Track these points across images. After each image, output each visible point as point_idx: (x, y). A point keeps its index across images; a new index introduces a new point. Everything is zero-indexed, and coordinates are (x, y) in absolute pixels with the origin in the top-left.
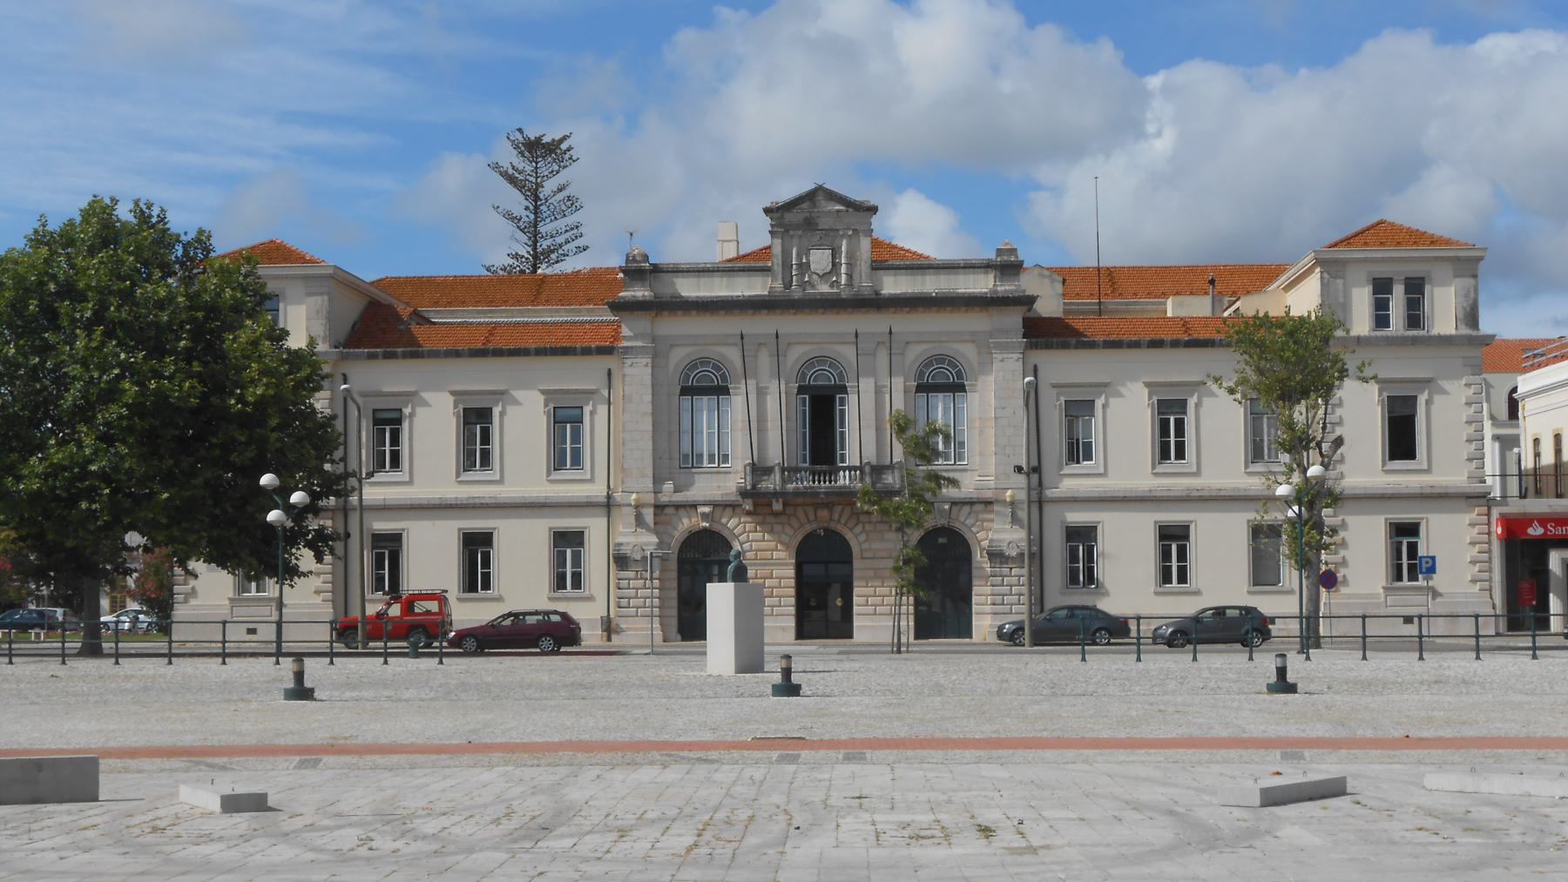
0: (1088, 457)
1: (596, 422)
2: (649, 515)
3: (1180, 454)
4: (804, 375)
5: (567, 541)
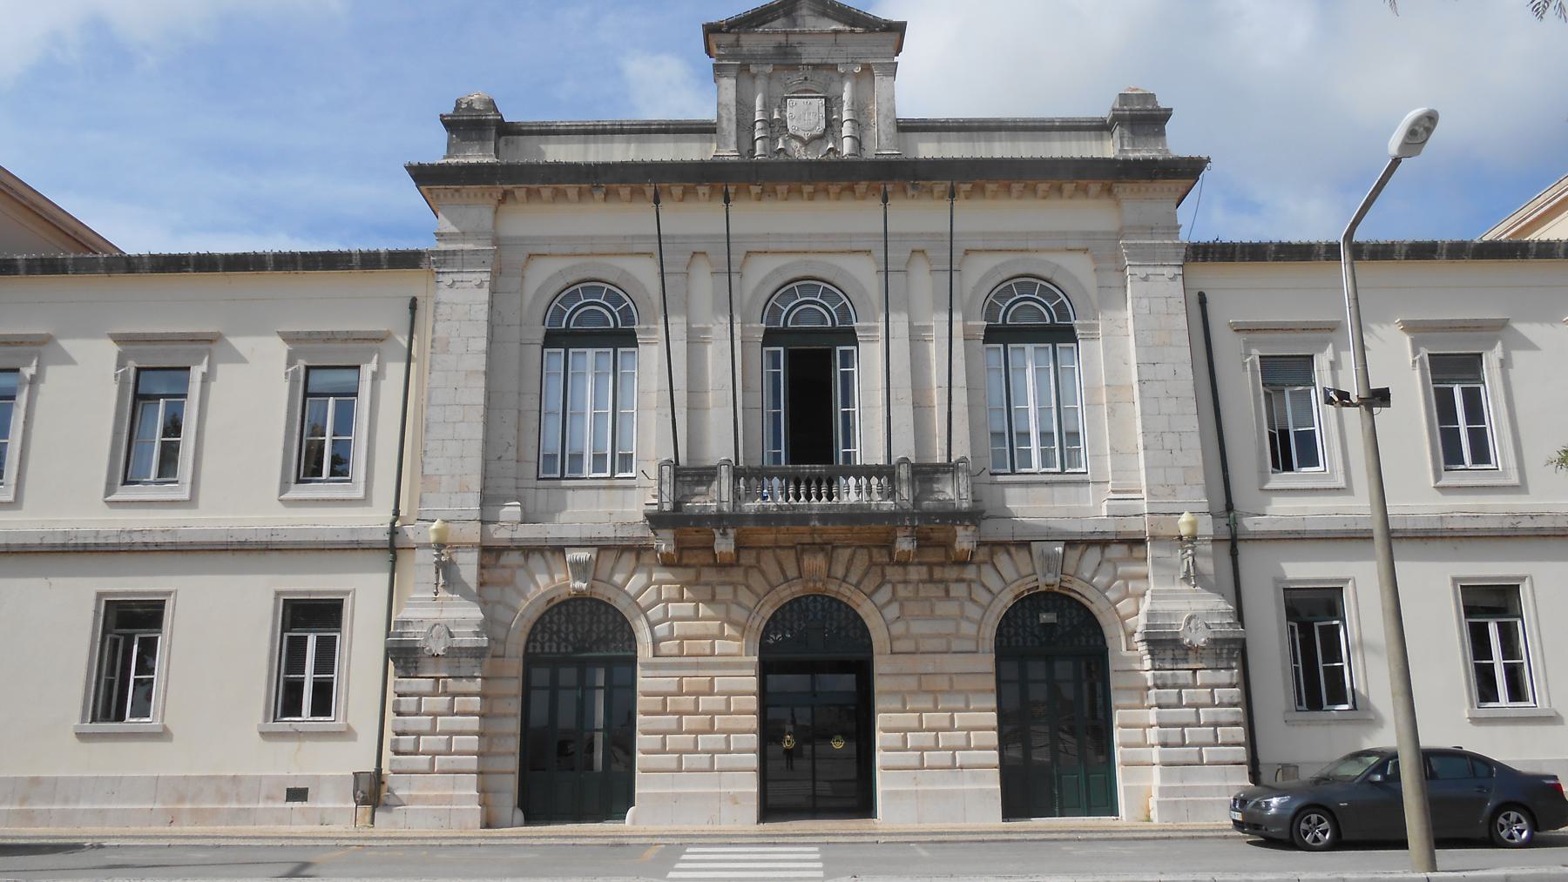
0: (1309, 458)
1: (381, 395)
2: (468, 565)
3: (1481, 453)
4: (775, 311)
5: (310, 620)
